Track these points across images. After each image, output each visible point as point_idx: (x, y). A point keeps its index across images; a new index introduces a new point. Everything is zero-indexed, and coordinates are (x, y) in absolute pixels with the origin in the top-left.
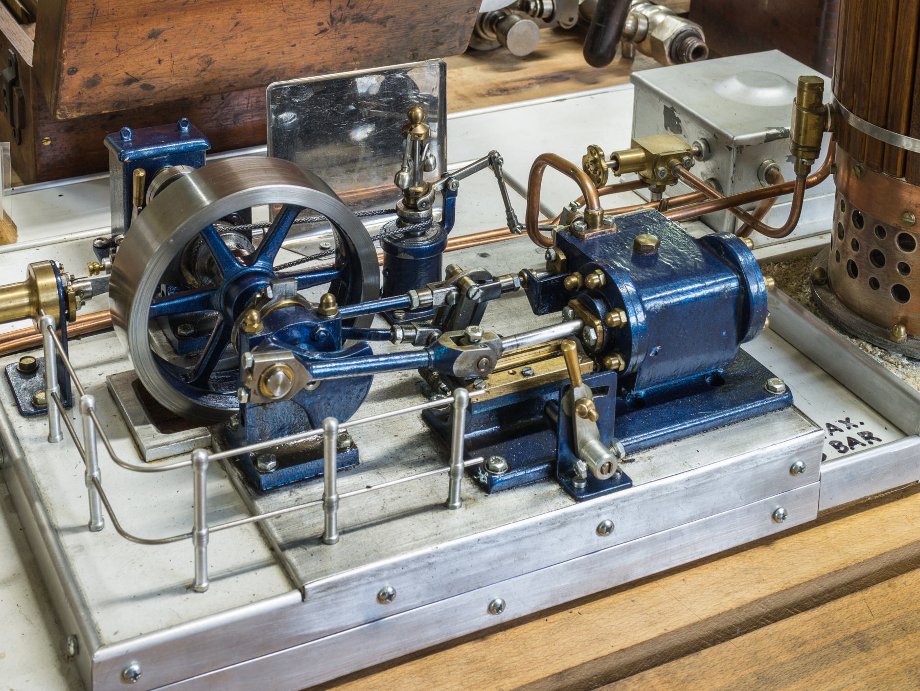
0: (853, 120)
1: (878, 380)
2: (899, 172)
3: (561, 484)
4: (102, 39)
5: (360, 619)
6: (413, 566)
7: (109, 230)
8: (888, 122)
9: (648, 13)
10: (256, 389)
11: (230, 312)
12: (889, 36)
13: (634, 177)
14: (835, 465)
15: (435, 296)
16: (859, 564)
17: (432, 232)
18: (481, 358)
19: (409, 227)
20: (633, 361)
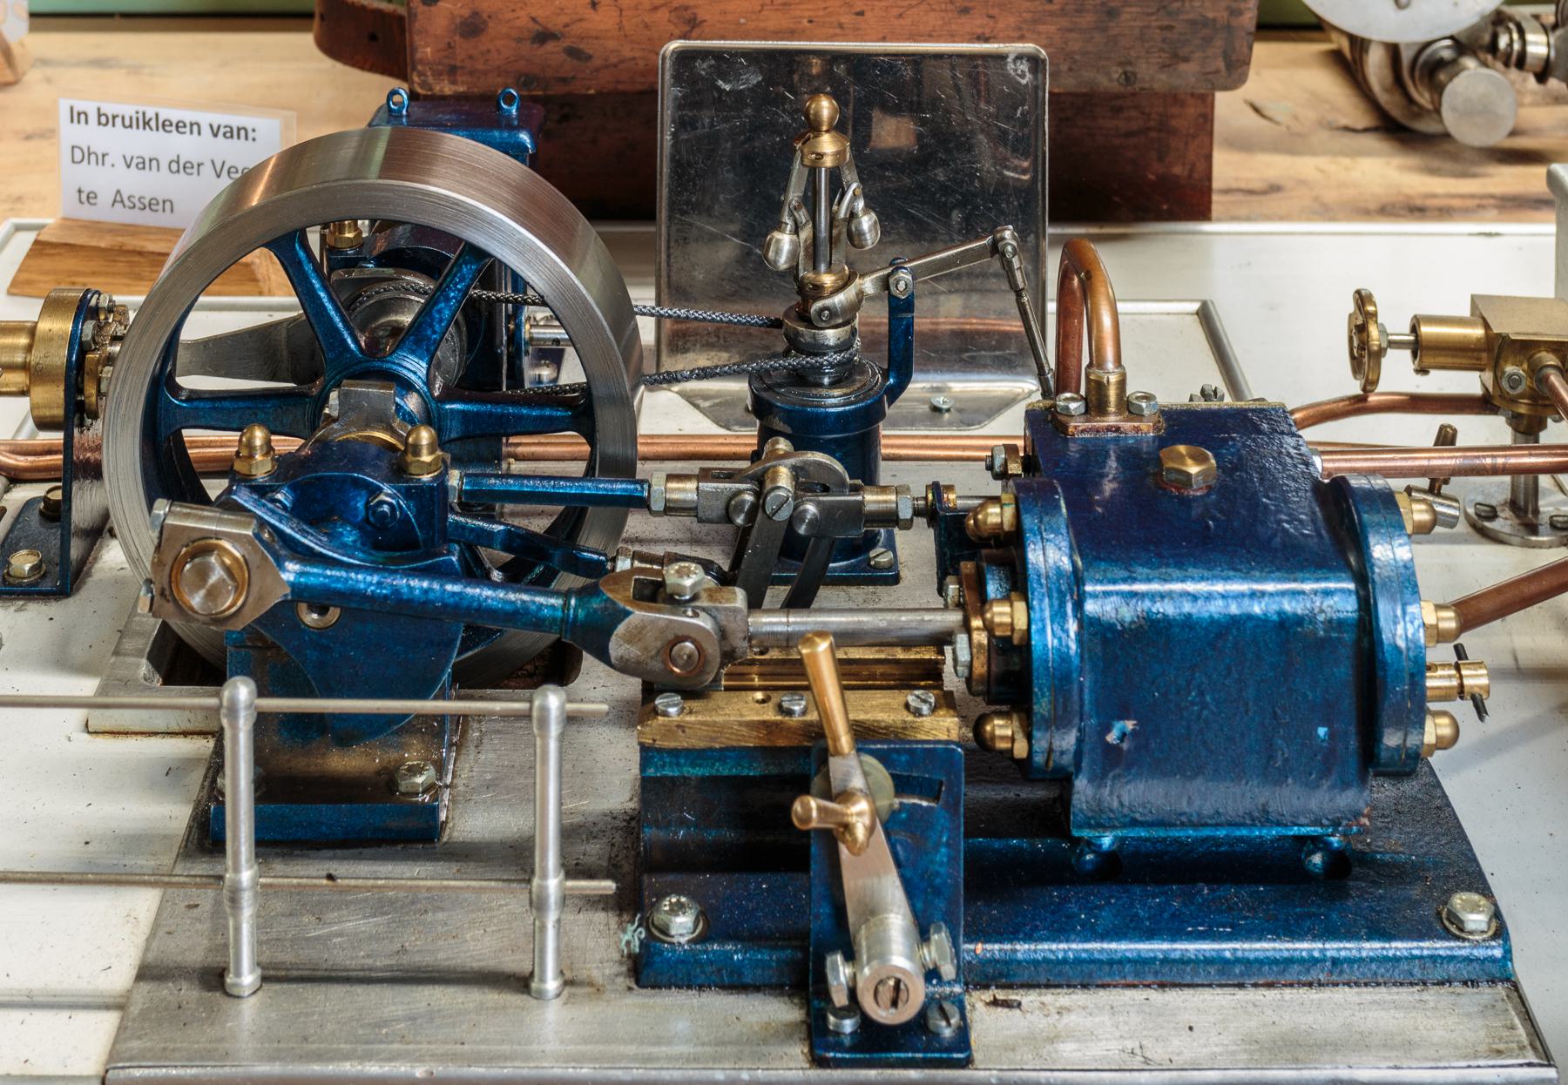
10: (166, 587)
13: (1469, 383)
18: (680, 639)
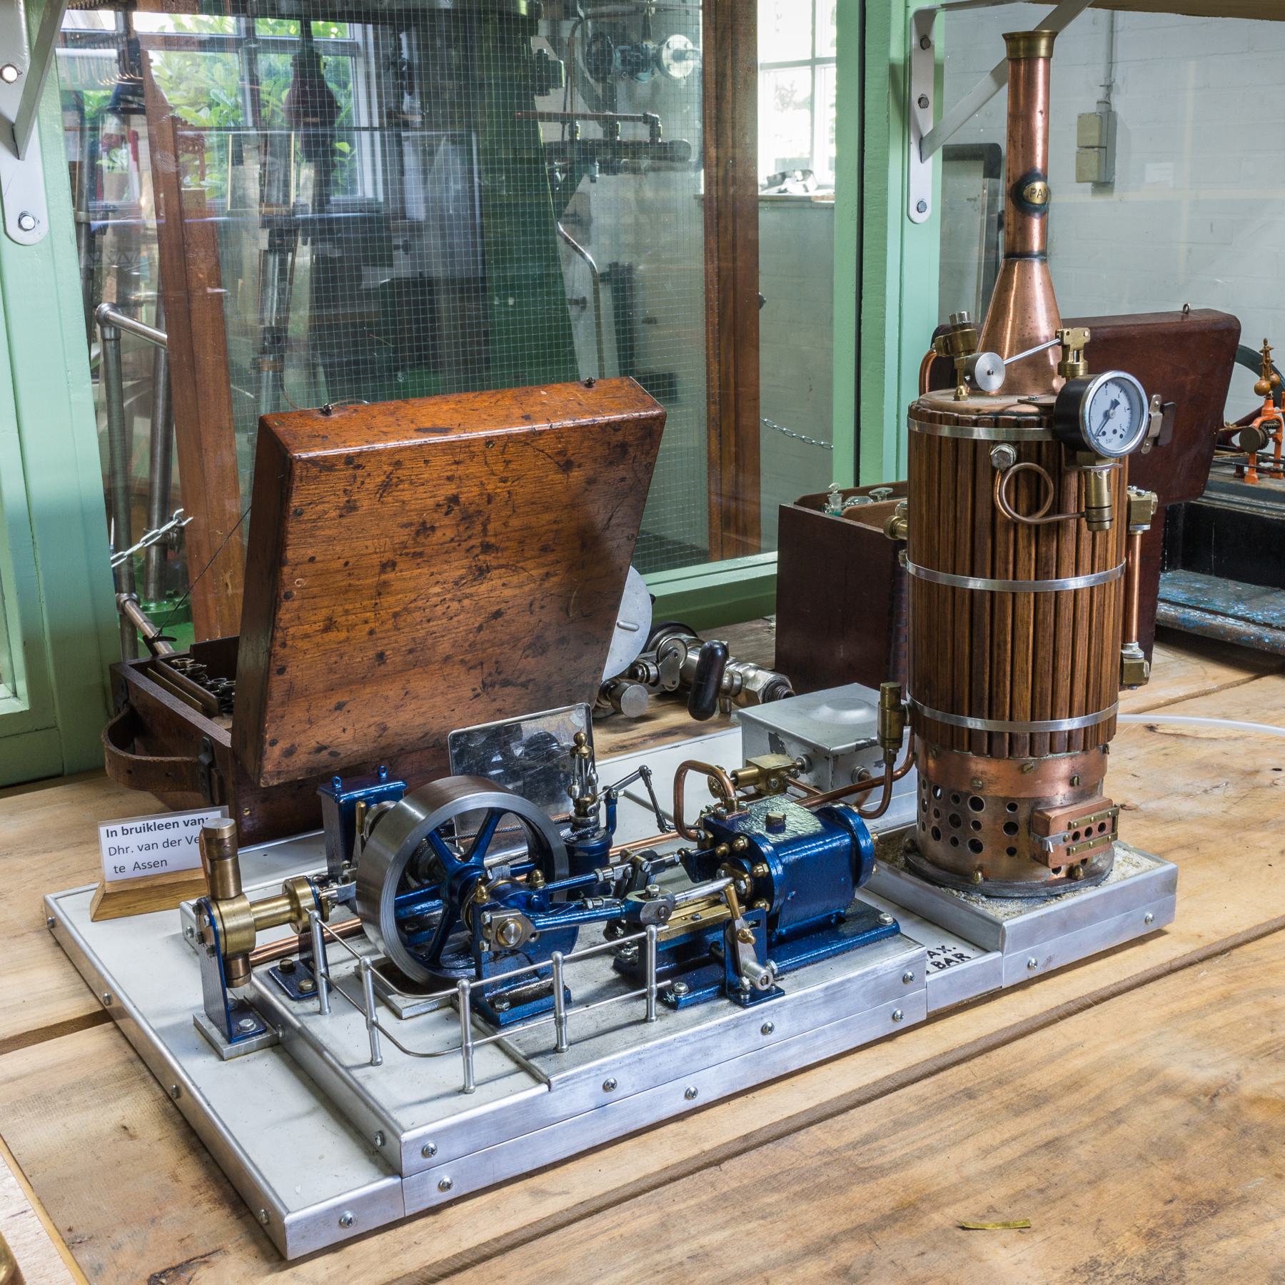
0: (927, 712)
1: (964, 915)
2: (966, 747)
3: (730, 998)
4: (298, 713)
5: (592, 1106)
6: (627, 1062)
7: (326, 869)
8: (955, 708)
9: (741, 670)
11: (456, 899)
12: (949, 639)
14: (936, 975)
15: (612, 873)
16: (962, 1047)
17: (599, 835)
19: (582, 831)
20: (775, 905)
